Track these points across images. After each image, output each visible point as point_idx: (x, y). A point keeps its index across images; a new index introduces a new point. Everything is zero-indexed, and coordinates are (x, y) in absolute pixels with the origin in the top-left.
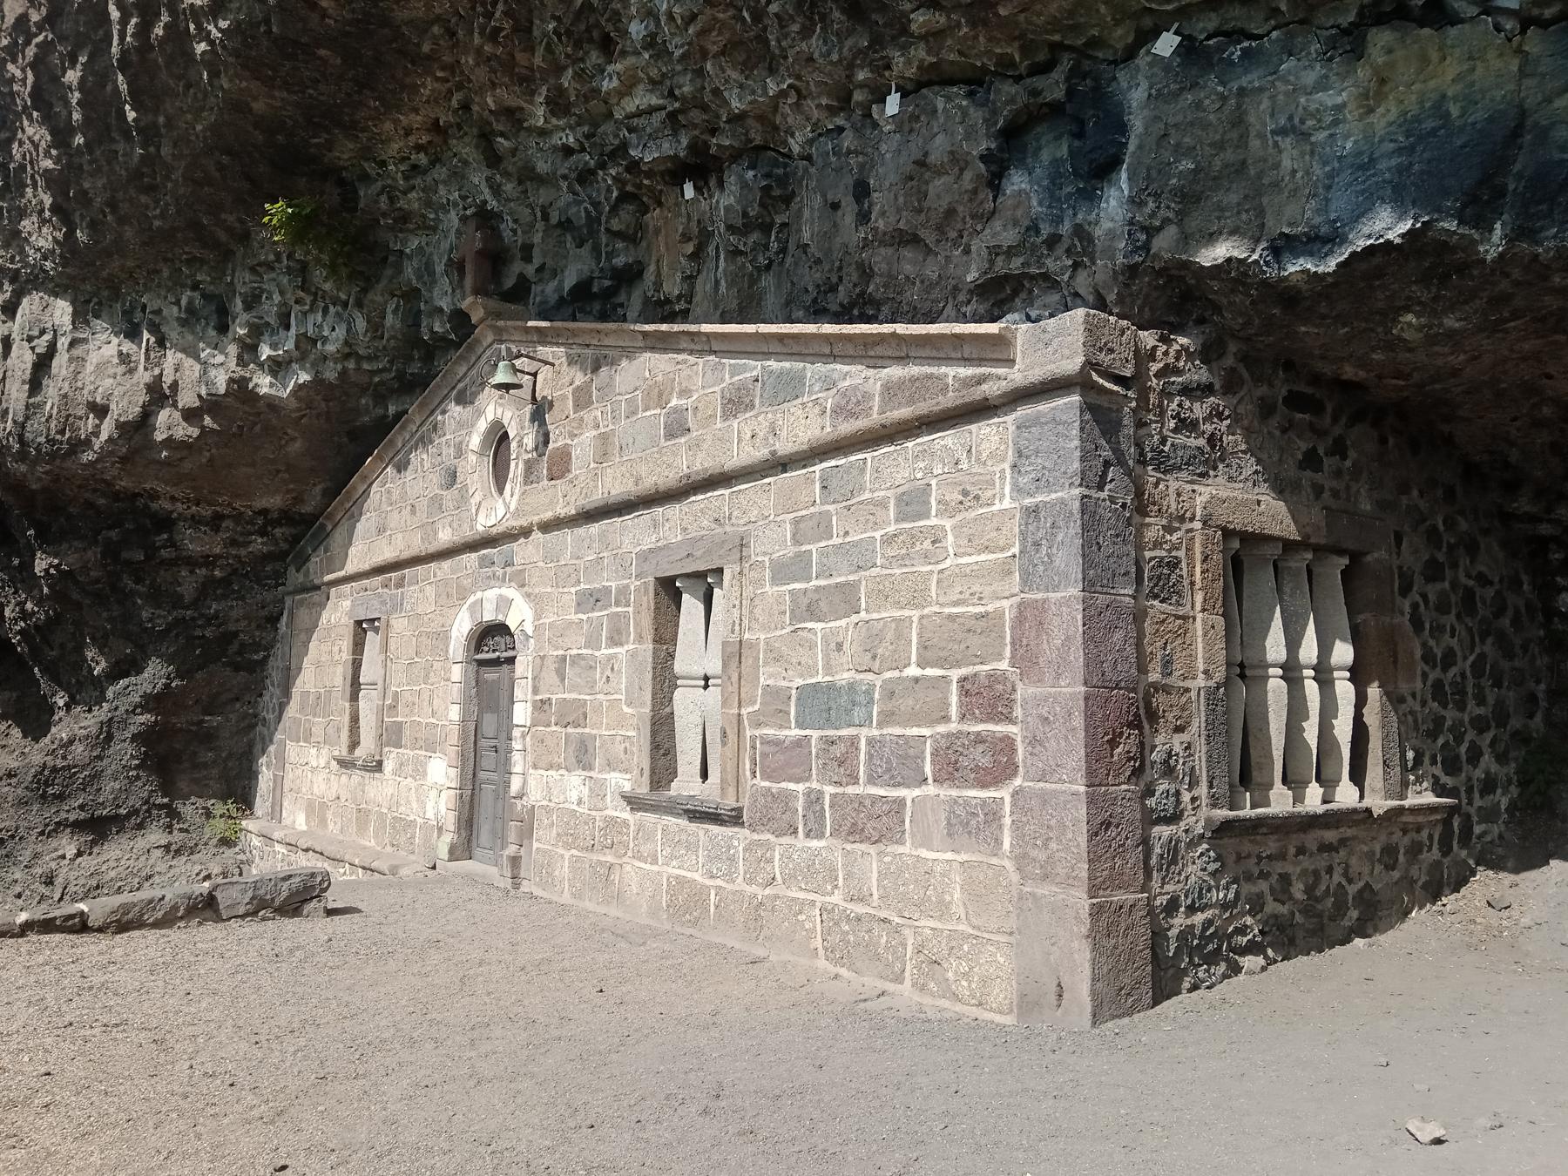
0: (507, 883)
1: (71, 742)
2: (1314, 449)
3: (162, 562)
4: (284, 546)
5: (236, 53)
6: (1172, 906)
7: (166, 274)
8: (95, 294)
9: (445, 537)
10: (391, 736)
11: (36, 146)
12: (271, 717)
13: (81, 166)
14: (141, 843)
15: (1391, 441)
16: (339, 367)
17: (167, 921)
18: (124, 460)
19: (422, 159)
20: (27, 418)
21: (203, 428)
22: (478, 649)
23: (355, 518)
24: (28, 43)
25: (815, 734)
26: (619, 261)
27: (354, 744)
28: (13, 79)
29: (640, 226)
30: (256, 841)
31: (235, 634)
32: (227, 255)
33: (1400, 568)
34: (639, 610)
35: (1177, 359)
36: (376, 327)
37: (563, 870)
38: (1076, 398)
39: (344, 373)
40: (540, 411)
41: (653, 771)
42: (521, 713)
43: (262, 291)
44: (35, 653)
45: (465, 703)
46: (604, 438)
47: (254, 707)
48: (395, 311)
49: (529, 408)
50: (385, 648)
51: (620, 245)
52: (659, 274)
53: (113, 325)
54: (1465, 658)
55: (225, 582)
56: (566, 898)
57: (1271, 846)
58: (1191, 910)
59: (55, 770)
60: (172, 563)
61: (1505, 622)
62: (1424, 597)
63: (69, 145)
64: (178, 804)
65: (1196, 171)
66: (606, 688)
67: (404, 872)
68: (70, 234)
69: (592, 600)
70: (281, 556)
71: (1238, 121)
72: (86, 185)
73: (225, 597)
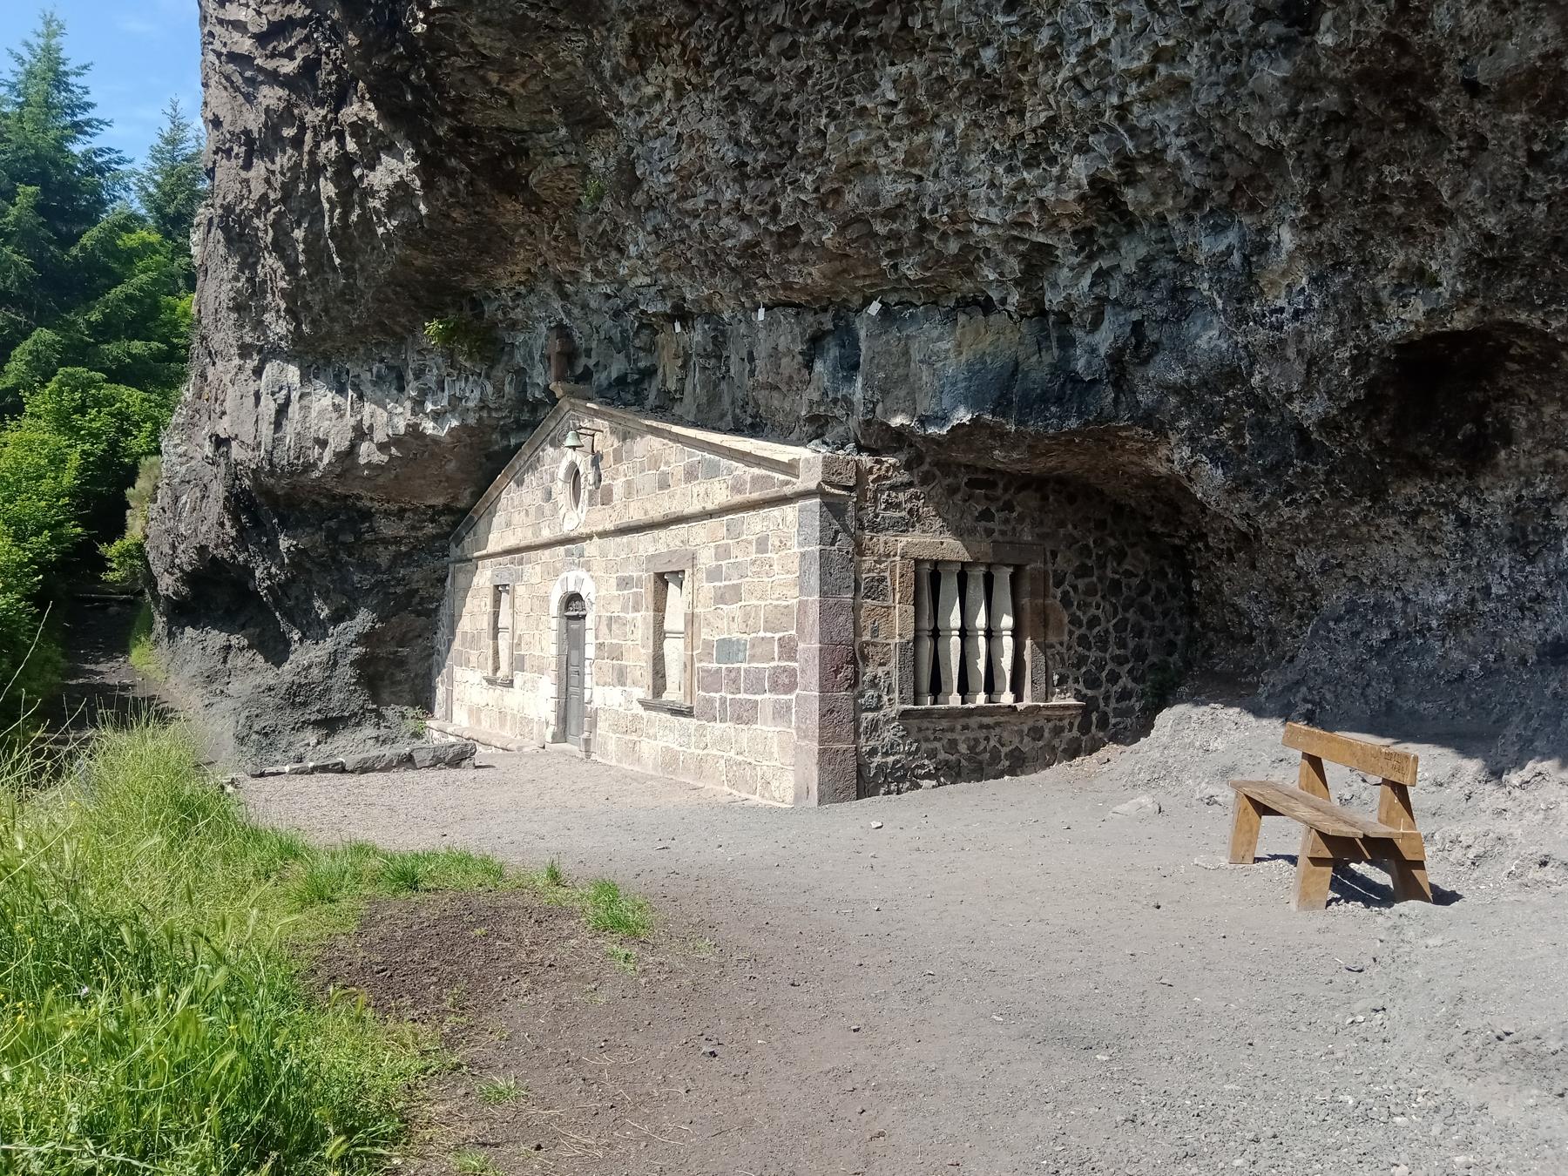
0: (582, 755)
1: (310, 666)
2: (988, 509)
3: (366, 542)
4: (448, 529)
5: (403, 238)
6: (873, 752)
7: (361, 350)
8: (314, 362)
9: (546, 535)
10: (518, 663)
11: (275, 272)
12: (443, 649)
13: (305, 287)
14: (359, 736)
15: (1051, 498)
16: (477, 416)
17: (387, 768)
18: (338, 476)
19: (522, 289)
20: (274, 448)
21: (390, 455)
22: (567, 609)
23: (492, 514)
24: (268, 210)
25: (724, 666)
26: (642, 365)
27: (496, 669)
28: (258, 228)
29: (653, 343)
30: (436, 735)
31: (417, 591)
32: (402, 340)
33: (1055, 571)
34: (647, 591)
35: (887, 471)
36: (499, 391)
37: (612, 747)
38: (818, 500)
39: (480, 419)
40: (596, 460)
41: (654, 687)
42: (590, 651)
43: (426, 366)
44: (278, 603)
45: (560, 642)
46: (629, 484)
47: (432, 642)
48: (510, 383)
49: (590, 457)
50: (513, 606)
51: (642, 354)
52: (665, 375)
53: (328, 384)
54: (1109, 621)
55: (409, 554)
56: (614, 763)
57: (945, 724)
58: (886, 754)
59: (300, 686)
60: (372, 543)
61: (1148, 599)
62: (1075, 588)
63: (297, 274)
64: (383, 709)
65: (886, 378)
66: (632, 637)
67: (525, 750)
68: (298, 327)
69: (624, 583)
70: (446, 536)
71: (906, 353)
72: (309, 298)
73: (408, 565)
